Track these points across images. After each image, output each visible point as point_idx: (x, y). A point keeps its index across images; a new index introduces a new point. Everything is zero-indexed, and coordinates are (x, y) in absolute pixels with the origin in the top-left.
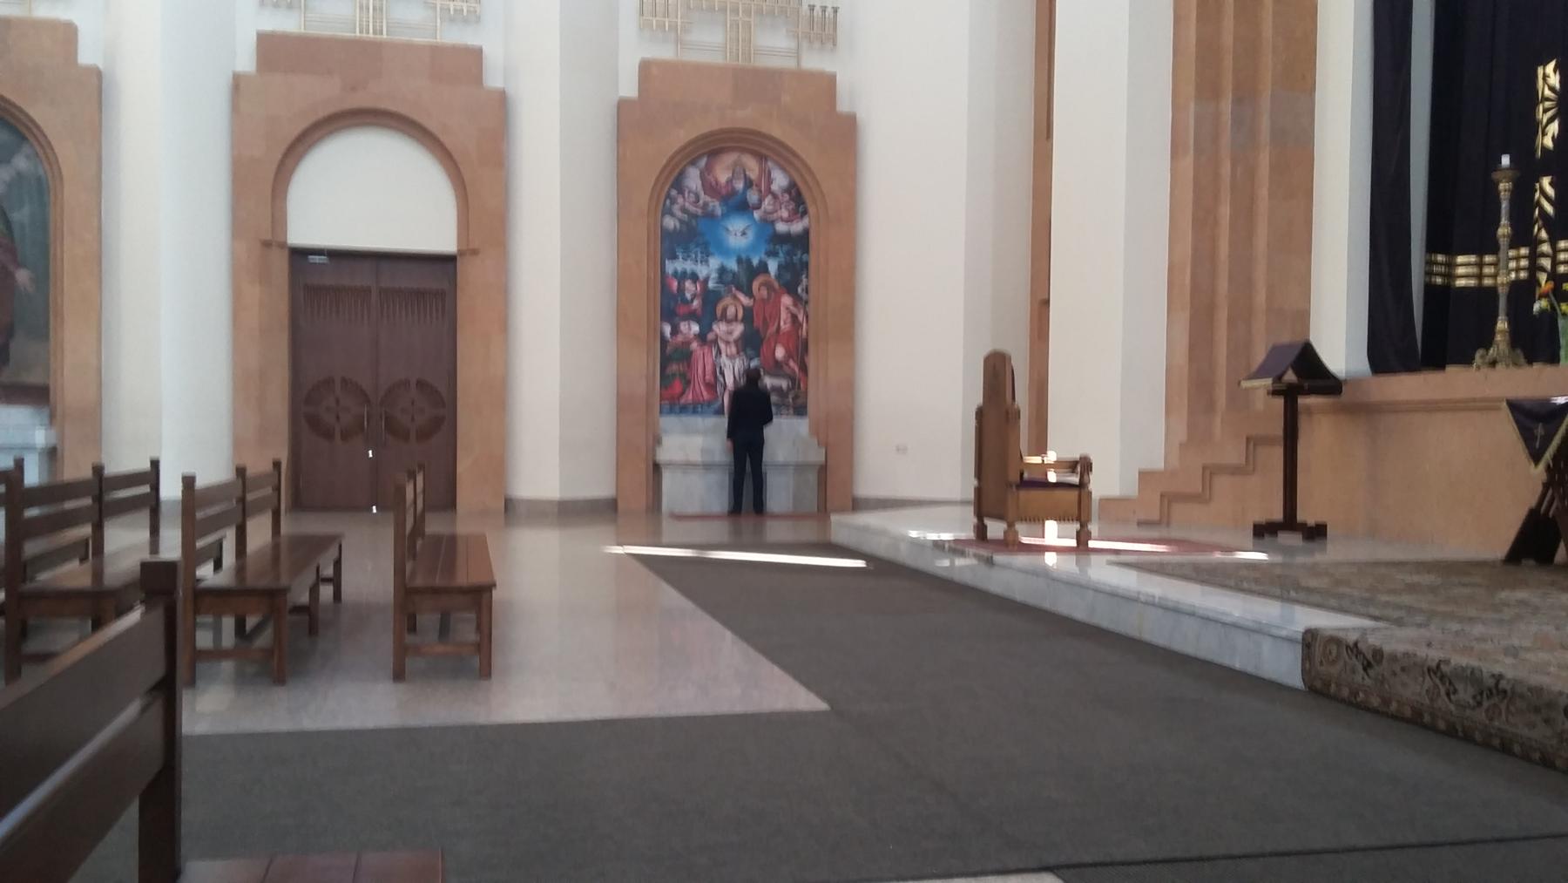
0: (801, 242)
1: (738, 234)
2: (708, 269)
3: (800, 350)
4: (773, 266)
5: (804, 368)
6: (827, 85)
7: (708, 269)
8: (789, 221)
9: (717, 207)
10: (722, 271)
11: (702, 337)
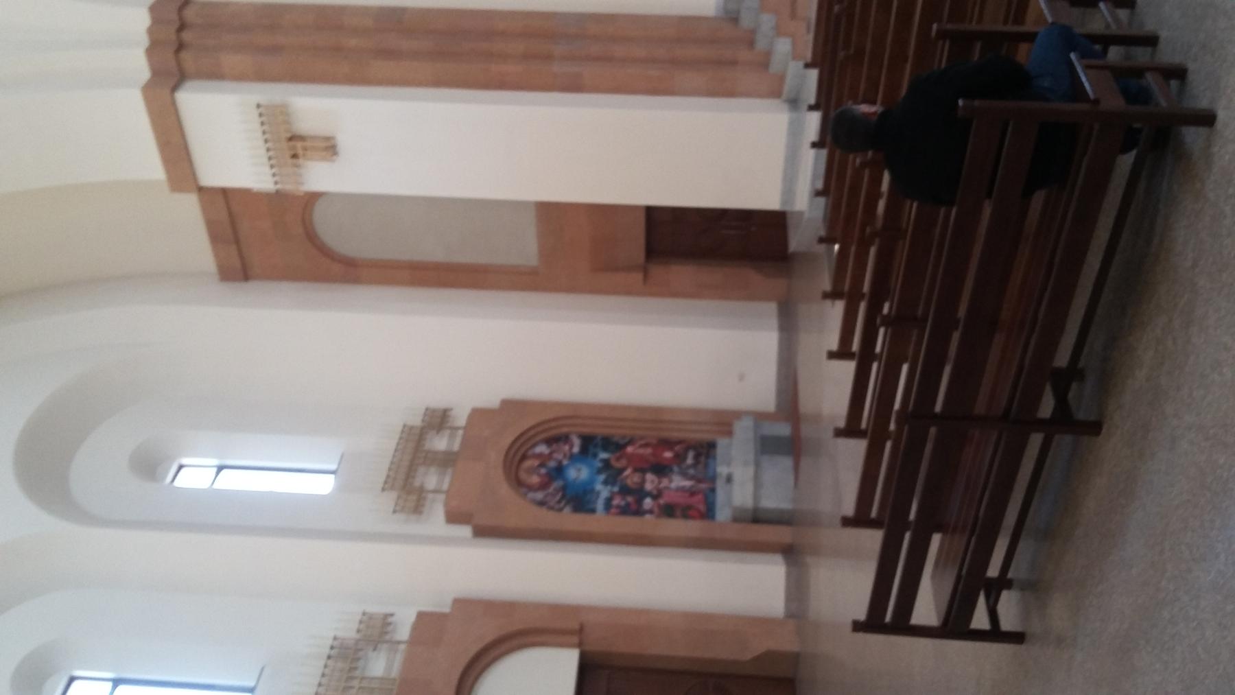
0: (588, 443)
1: (579, 473)
2: (604, 492)
3: (667, 443)
4: (603, 455)
5: (680, 442)
6: (479, 415)
7: (604, 492)
8: (571, 447)
9: (558, 484)
10: (606, 483)
11: (655, 497)
